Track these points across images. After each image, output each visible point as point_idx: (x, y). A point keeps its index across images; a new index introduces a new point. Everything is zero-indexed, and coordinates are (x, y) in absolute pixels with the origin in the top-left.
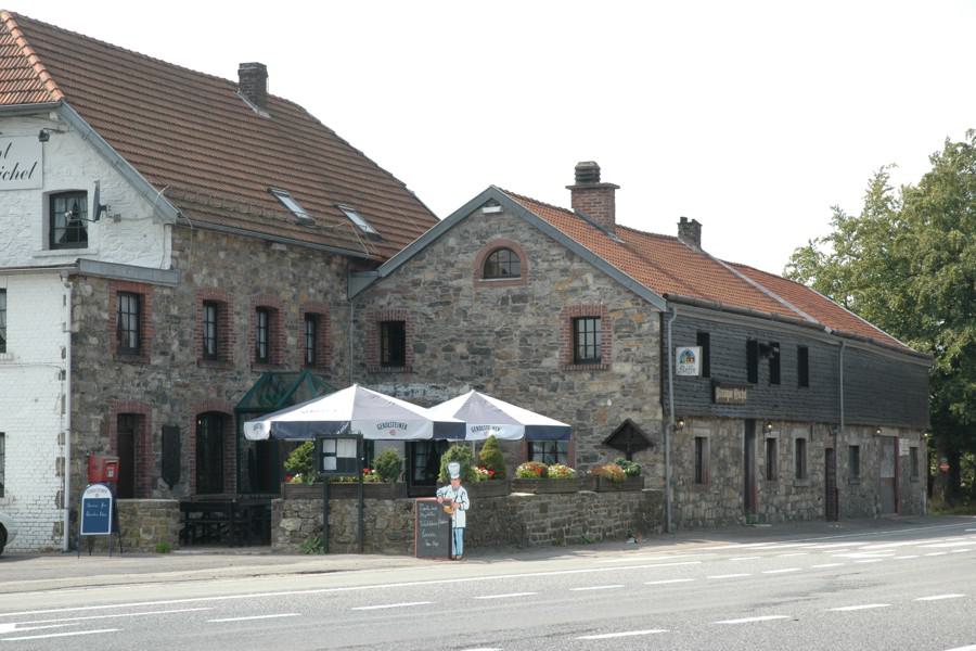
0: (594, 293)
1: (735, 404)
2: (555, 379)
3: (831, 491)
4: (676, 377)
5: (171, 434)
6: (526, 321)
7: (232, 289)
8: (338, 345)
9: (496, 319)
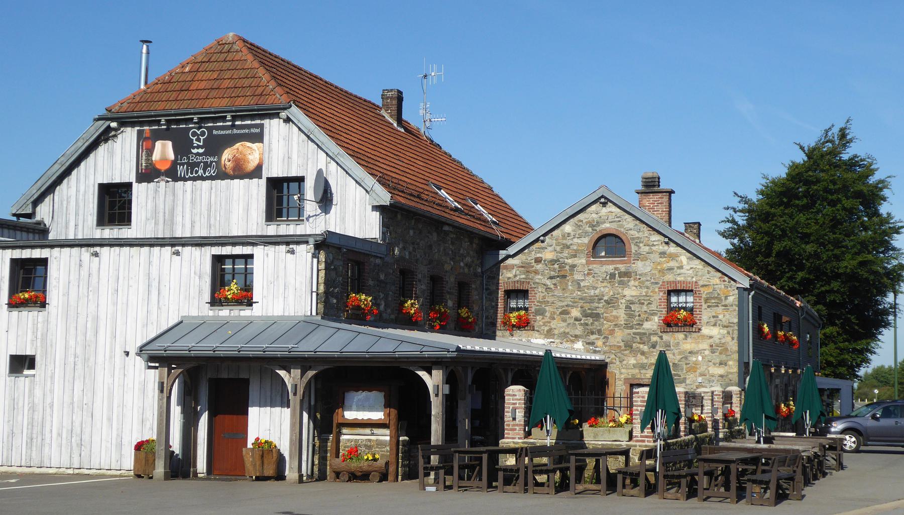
6: (631, 292)
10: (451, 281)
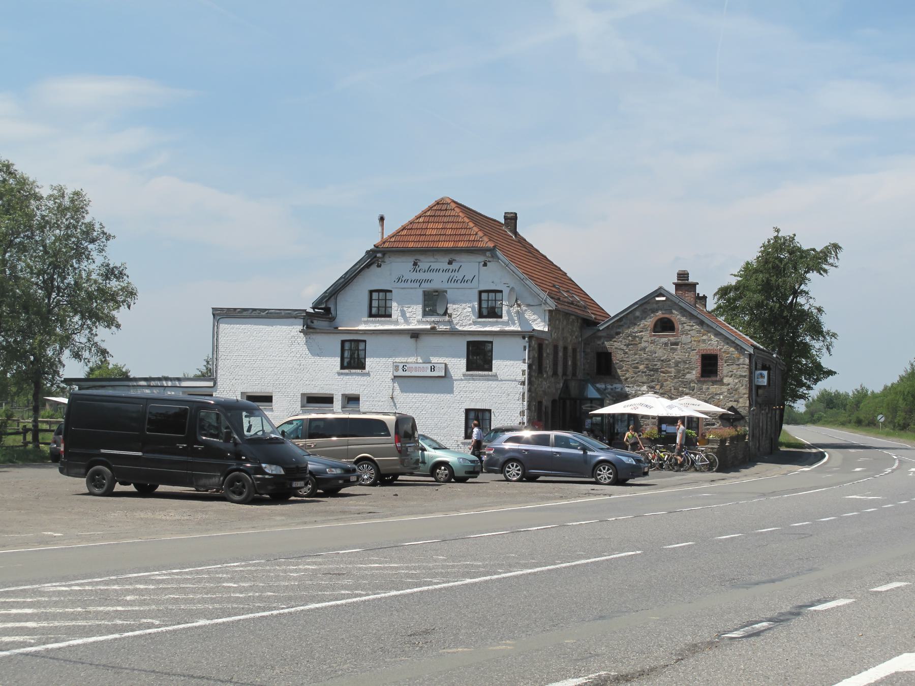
2: (692, 385)
6: (678, 355)
9: (661, 353)
10: (570, 348)
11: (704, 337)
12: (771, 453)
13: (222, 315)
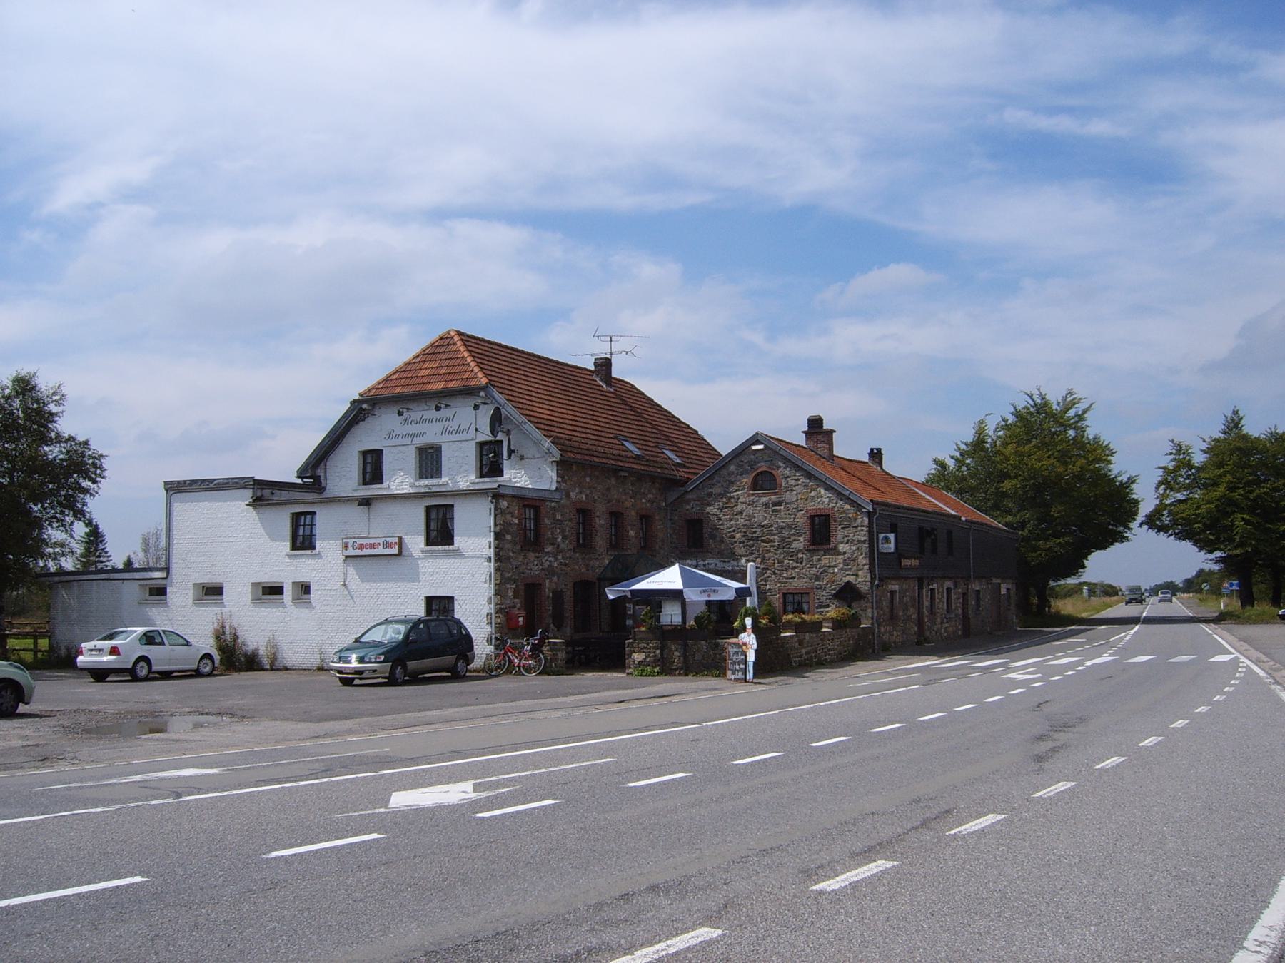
0: (824, 500)
1: (912, 568)
3: (965, 618)
4: (879, 553)
5: (558, 596)
7: (595, 501)
8: (661, 535)
9: (760, 516)
11: (813, 494)
12: (919, 643)
13: (175, 488)
